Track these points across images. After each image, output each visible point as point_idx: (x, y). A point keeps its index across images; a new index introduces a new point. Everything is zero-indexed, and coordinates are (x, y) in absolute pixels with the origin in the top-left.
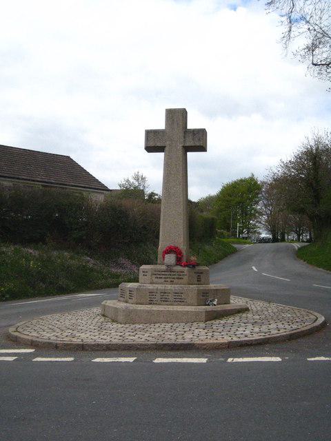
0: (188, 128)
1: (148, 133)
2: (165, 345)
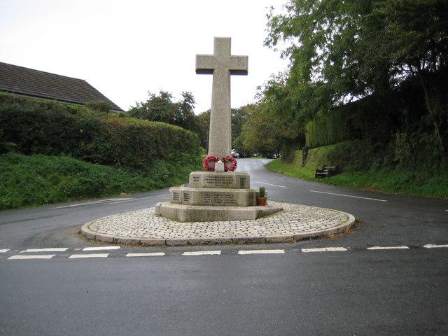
0: (232, 54)
1: (199, 58)
2: (240, 239)
